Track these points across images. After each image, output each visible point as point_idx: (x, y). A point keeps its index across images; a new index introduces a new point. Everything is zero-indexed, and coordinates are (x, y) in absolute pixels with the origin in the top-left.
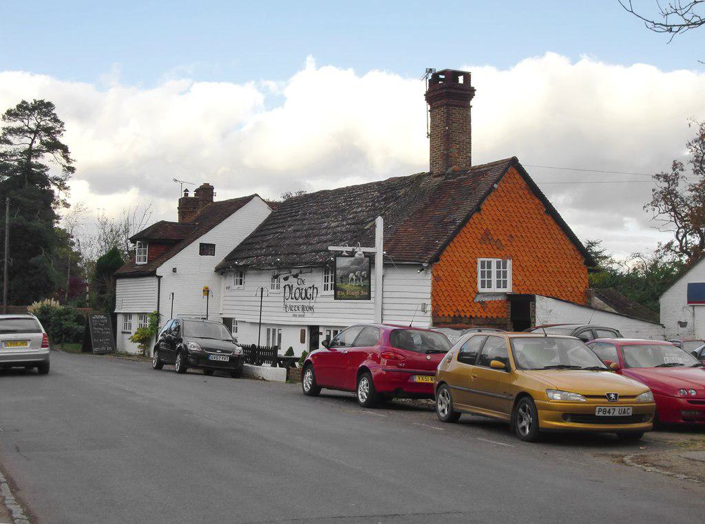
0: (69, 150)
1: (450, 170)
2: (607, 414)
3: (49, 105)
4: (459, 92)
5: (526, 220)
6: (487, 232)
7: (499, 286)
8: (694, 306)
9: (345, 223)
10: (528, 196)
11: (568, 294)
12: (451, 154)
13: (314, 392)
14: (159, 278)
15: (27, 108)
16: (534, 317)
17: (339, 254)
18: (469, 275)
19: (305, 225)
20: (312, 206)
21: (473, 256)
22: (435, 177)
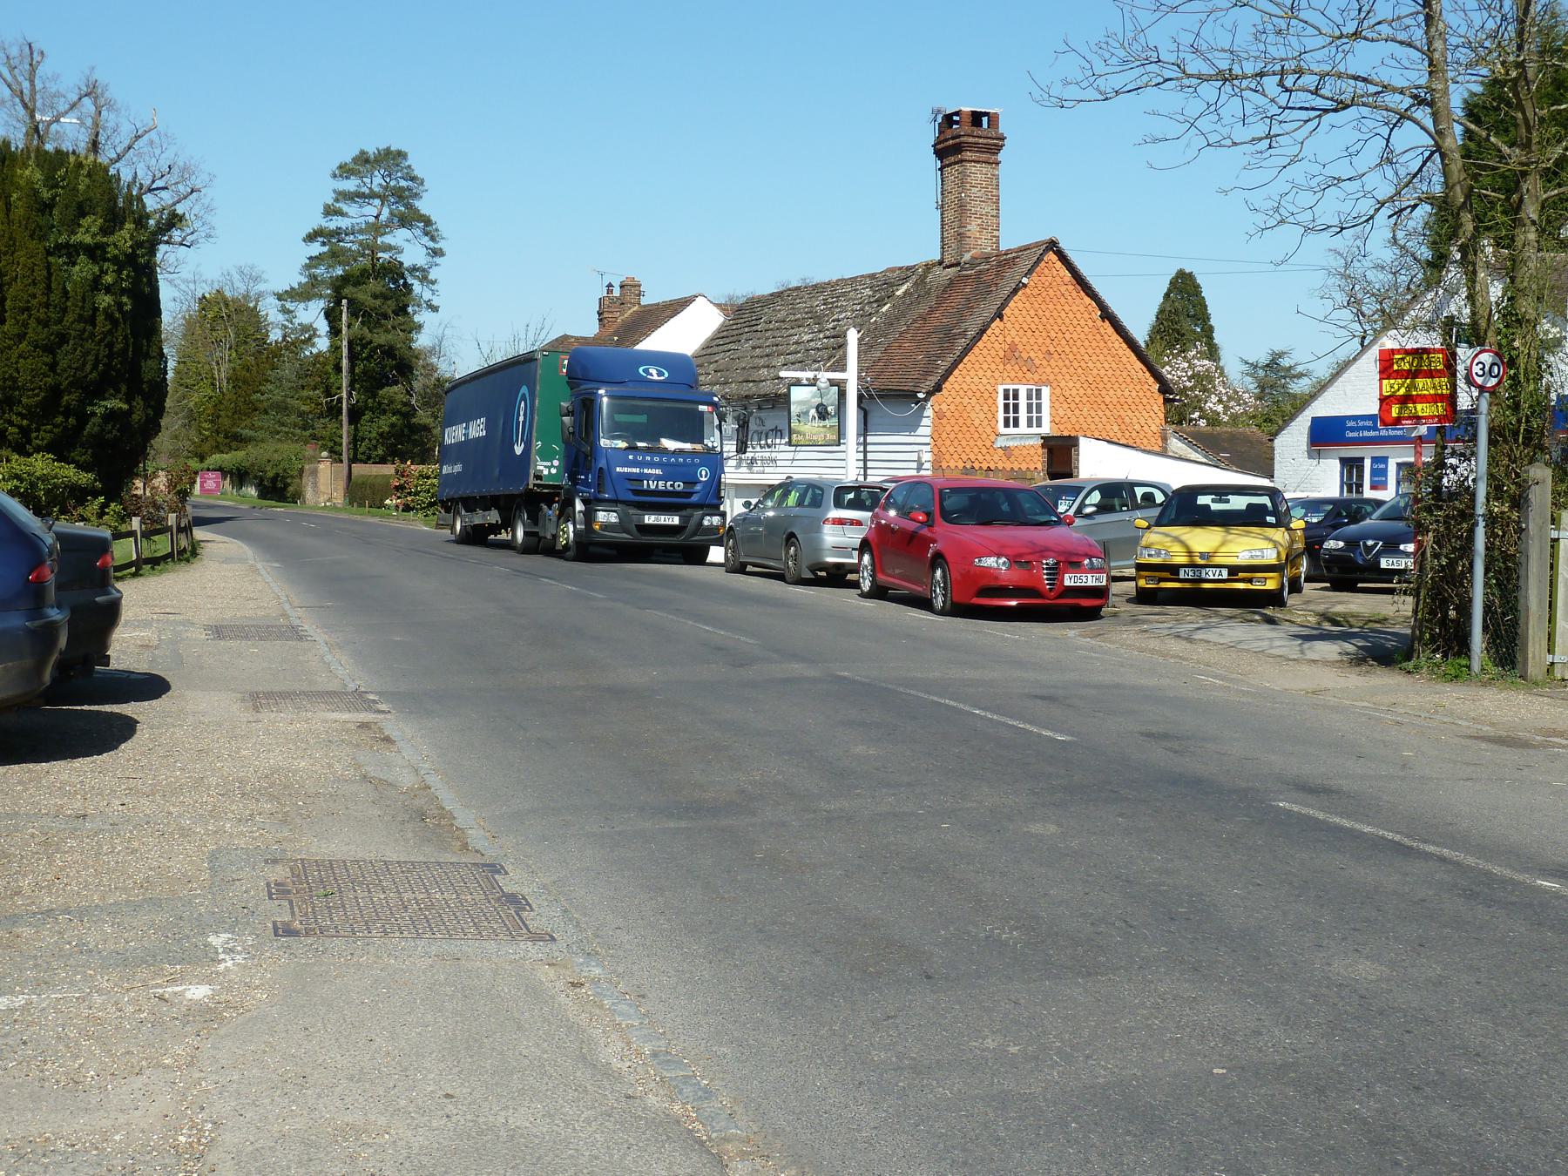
0: (433, 219)
1: (967, 257)
3: (401, 155)
4: (981, 141)
5: (1071, 328)
6: (1013, 348)
7: (1030, 425)
9: (821, 336)
10: (1074, 294)
11: (1134, 434)
12: (968, 234)
15: (367, 161)
17: (798, 383)
18: (985, 408)
19: (767, 339)
20: (780, 310)
22: (948, 267)
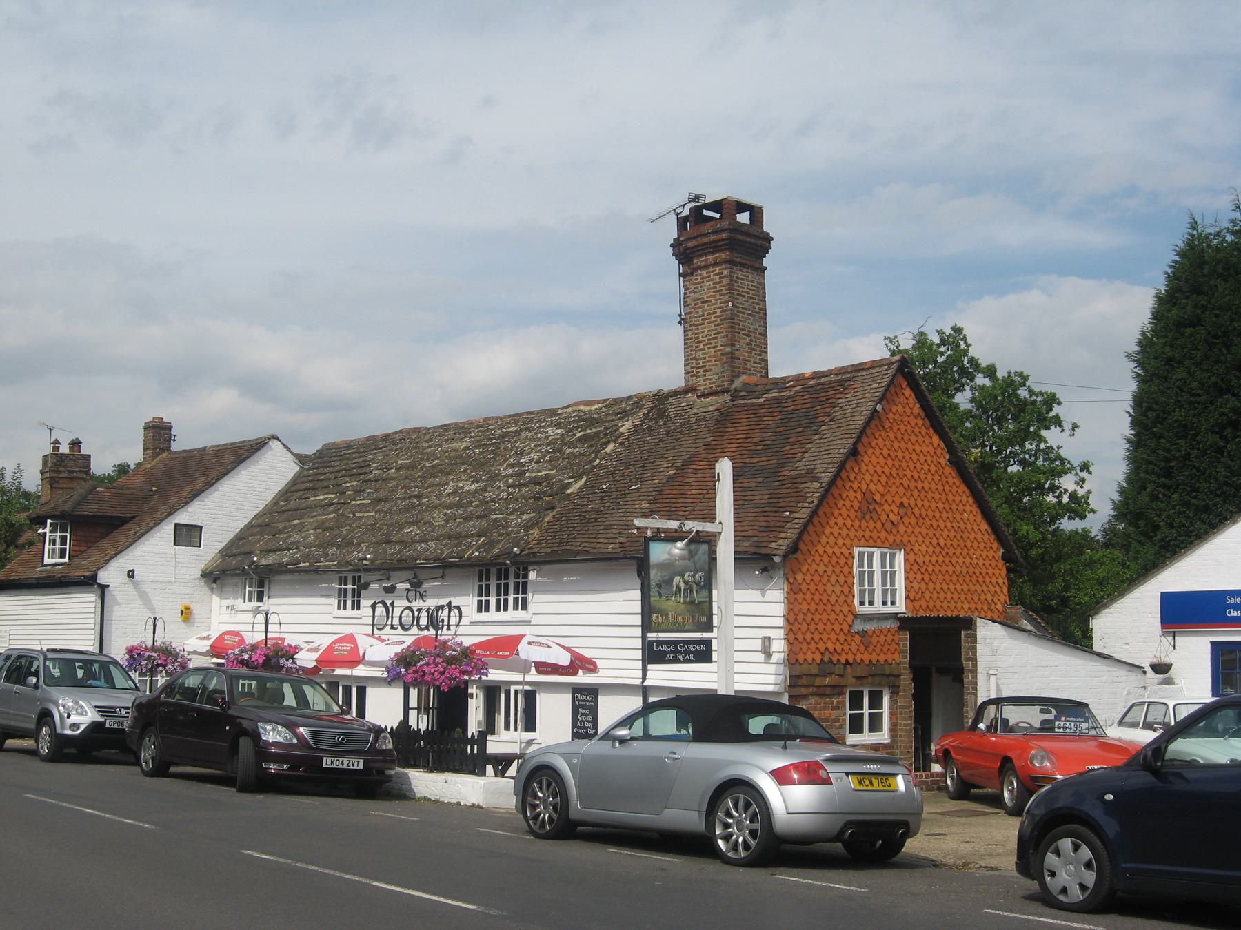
1: (737, 383)
2: (340, 766)
8: (1174, 632)
12: (737, 354)
13: (160, 770)
14: (103, 588)
16: (974, 660)
21: (848, 542)
22: (704, 395)
